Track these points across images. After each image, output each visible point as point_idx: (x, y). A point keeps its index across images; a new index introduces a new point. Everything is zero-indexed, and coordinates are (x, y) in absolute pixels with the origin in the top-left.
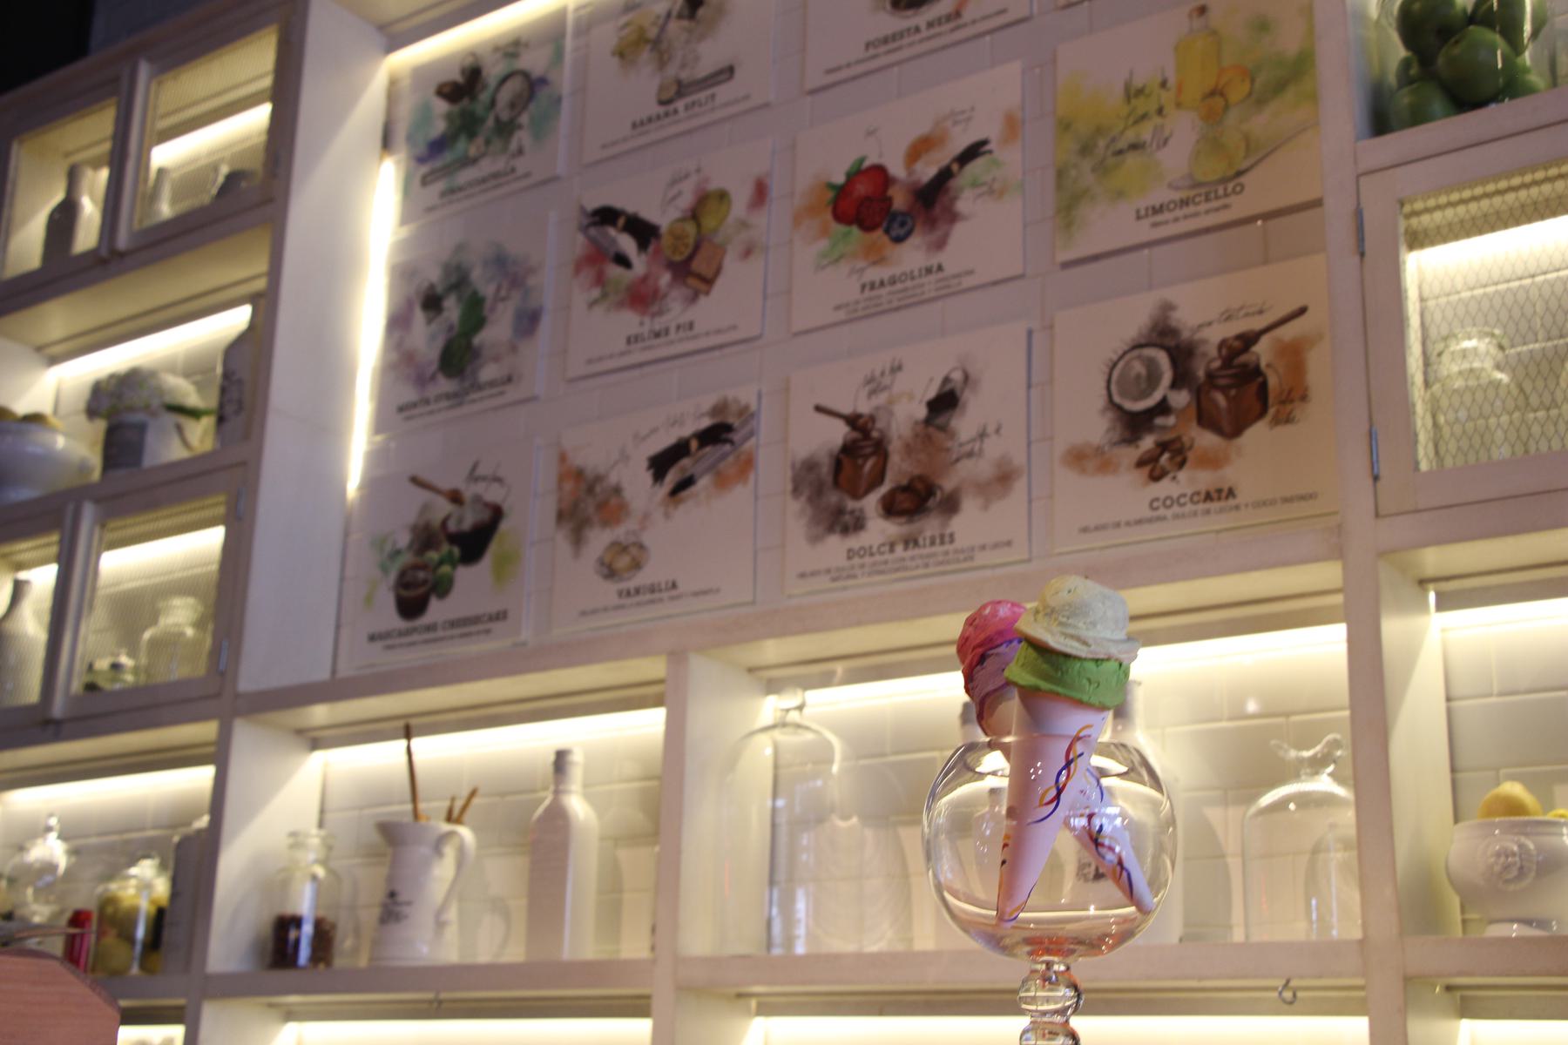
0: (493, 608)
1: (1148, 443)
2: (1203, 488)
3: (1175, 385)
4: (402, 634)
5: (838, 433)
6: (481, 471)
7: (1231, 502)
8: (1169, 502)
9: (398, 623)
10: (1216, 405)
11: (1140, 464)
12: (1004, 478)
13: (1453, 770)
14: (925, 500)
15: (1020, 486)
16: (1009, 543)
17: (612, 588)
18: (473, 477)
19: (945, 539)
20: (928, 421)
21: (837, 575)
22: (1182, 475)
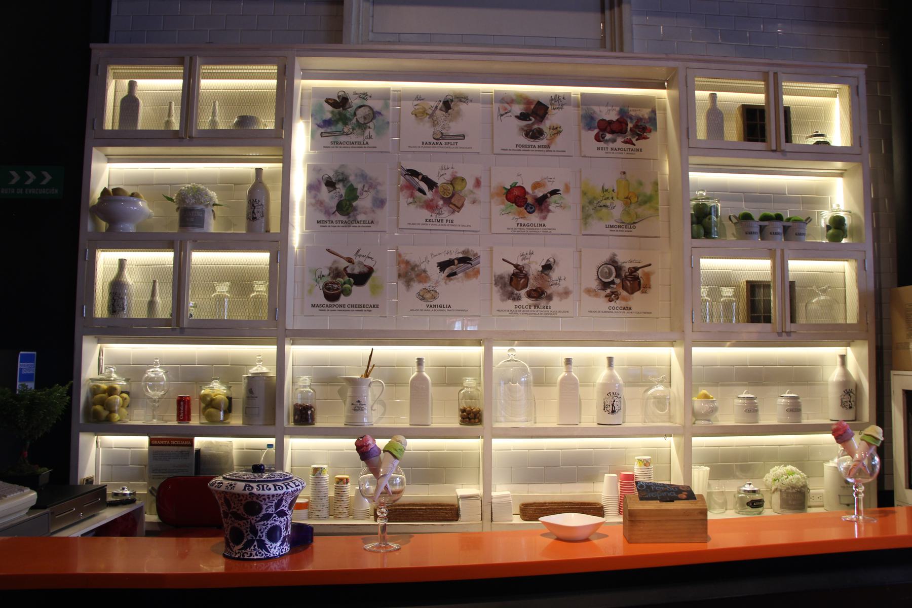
8: (614, 308)
11: (606, 296)
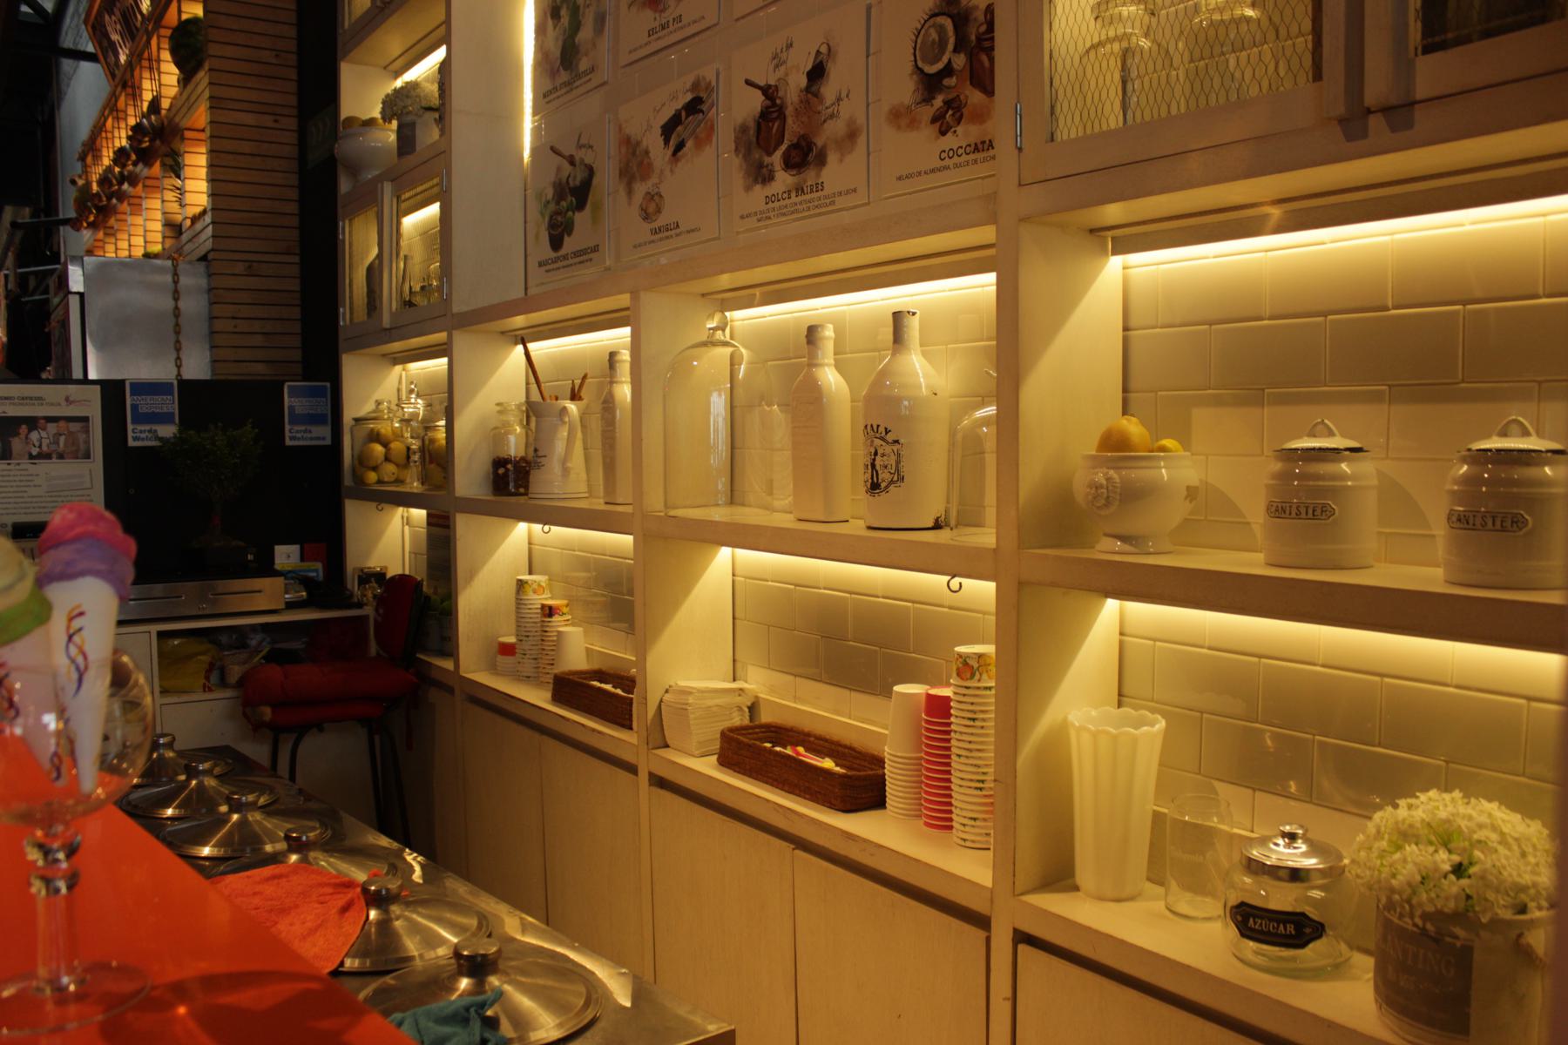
0: (591, 244)
1: (938, 102)
2: (972, 140)
3: (955, 51)
4: (555, 261)
5: (756, 100)
6: (583, 141)
7: (991, 152)
8: (953, 153)
9: (553, 255)
10: (982, 64)
11: (934, 120)
12: (852, 135)
13: (1125, 390)
14: (807, 155)
15: (862, 140)
16: (855, 190)
17: (647, 227)
18: (580, 147)
19: (819, 187)
20: (808, 89)
21: (763, 217)
22: (960, 129)
